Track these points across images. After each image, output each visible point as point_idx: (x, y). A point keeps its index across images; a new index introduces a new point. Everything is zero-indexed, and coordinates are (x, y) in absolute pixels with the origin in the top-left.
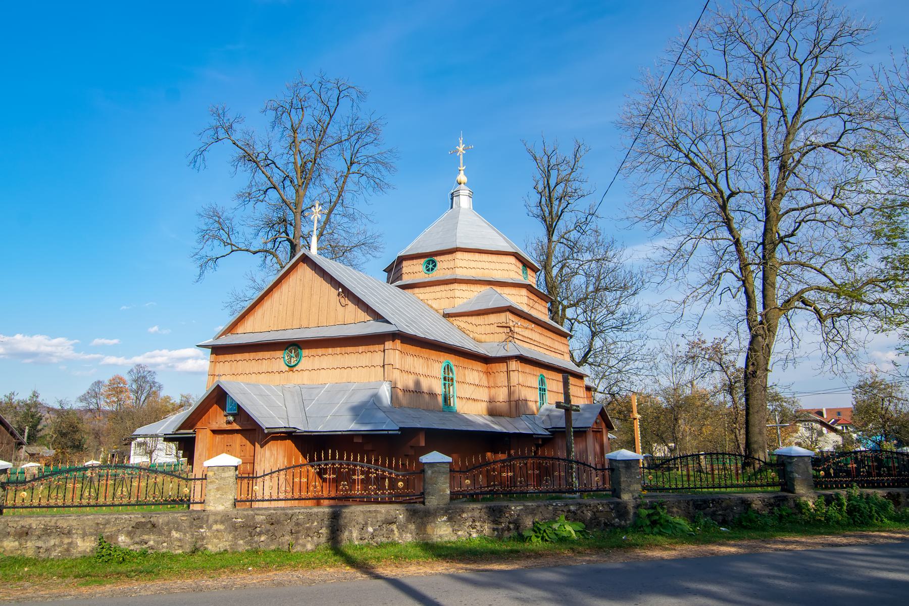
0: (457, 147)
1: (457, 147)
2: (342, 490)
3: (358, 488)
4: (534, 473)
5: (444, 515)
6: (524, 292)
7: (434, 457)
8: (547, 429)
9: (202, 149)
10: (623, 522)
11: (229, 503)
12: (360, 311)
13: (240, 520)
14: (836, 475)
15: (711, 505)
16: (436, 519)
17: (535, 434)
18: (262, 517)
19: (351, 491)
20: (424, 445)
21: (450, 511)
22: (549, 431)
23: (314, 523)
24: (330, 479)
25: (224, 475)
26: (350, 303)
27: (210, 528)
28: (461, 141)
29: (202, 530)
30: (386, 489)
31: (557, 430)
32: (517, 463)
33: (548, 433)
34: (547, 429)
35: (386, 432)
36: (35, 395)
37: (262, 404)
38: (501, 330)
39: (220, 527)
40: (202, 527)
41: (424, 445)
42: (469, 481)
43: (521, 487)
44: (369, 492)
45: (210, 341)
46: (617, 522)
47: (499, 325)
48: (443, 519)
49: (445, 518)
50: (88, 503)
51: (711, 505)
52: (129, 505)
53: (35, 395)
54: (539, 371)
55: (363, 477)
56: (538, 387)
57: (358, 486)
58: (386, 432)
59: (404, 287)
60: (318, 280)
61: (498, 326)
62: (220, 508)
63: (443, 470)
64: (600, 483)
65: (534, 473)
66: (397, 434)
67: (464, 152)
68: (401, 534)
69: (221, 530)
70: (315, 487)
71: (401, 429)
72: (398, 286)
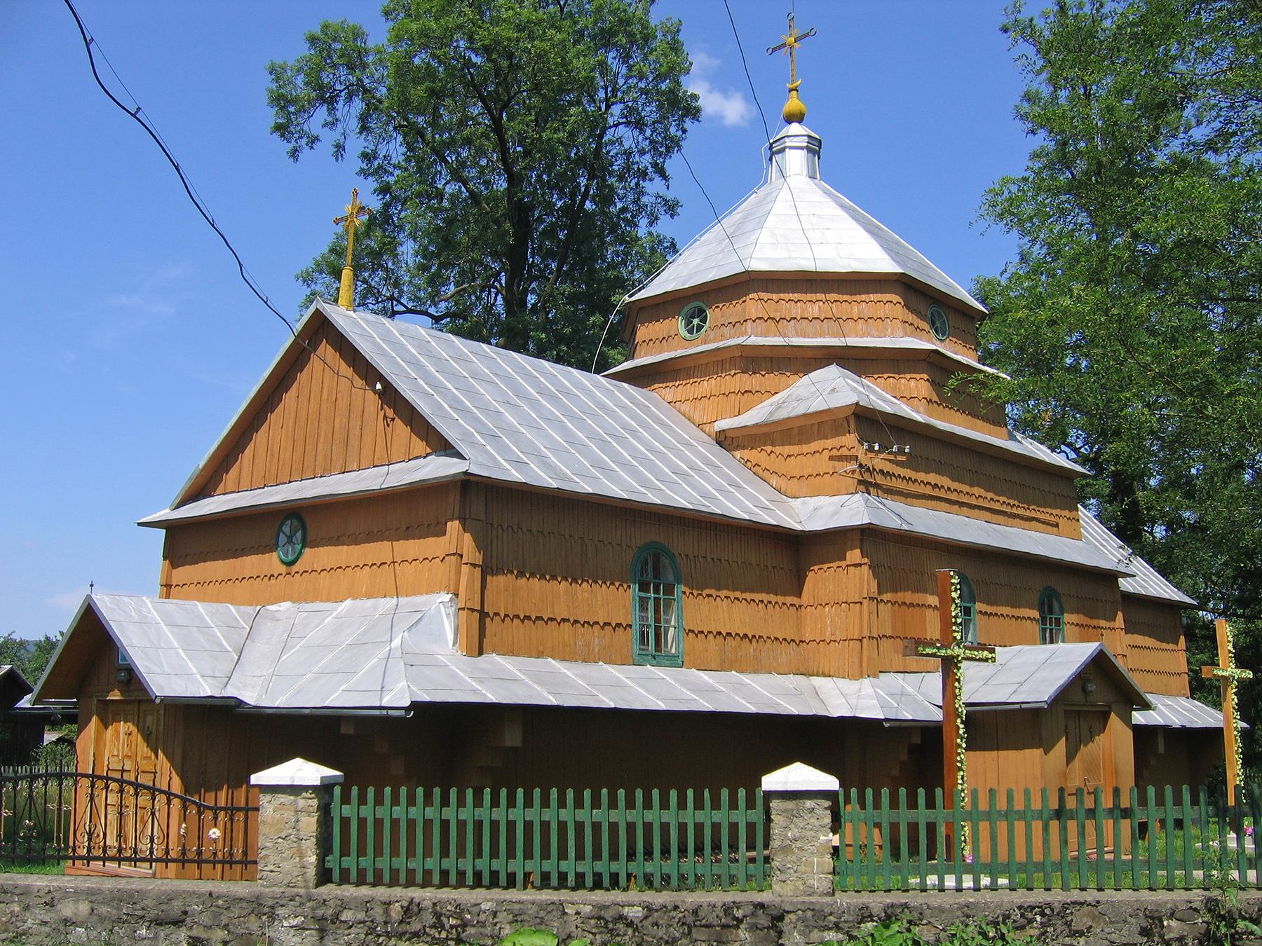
45: (166, 514)
47: (835, 453)
61: (831, 458)
71: (415, 705)
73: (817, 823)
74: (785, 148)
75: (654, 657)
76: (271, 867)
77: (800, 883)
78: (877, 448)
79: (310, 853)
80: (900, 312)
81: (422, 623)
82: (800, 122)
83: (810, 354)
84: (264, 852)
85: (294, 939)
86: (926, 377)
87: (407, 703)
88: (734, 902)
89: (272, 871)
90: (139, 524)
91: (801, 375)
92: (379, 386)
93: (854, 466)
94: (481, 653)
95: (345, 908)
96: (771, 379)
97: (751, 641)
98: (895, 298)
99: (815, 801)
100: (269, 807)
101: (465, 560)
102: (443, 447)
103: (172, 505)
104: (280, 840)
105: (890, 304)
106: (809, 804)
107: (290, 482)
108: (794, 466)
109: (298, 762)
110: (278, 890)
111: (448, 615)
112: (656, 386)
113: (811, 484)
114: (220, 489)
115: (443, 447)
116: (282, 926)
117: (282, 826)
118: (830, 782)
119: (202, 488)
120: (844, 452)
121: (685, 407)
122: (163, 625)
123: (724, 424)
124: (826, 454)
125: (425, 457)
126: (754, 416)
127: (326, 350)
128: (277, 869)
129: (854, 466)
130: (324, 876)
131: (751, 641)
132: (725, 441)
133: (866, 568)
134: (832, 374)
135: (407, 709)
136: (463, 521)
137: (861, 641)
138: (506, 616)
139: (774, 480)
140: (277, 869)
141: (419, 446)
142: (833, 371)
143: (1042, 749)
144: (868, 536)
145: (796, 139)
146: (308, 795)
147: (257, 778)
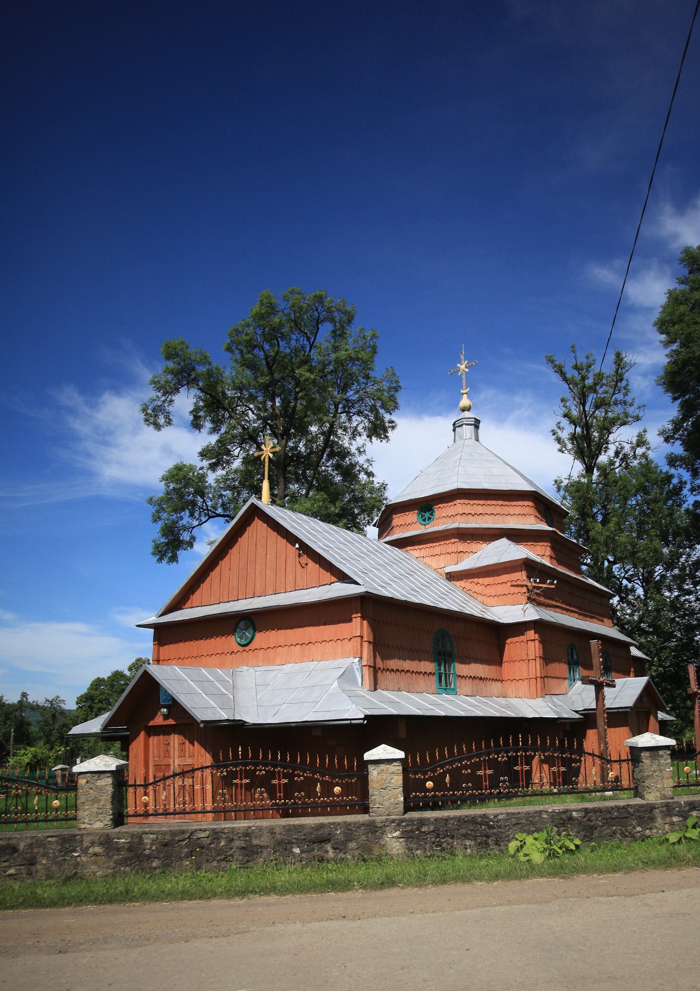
0: (459, 365)
1: (459, 365)
2: (259, 799)
7: (382, 751)
8: (577, 712)
11: (109, 819)
12: (322, 570)
13: (123, 840)
18: (151, 836)
19: (26, 813)
21: (404, 824)
22: (581, 714)
23: (220, 842)
24: (241, 784)
25: (99, 783)
26: (310, 561)
27: (85, 851)
28: (462, 357)
29: (76, 854)
31: (620, 710)
33: (577, 716)
34: (577, 712)
35: (349, 722)
36: (24, 695)
37: (201, 692)
38: (516, 590)
39: (97, 849)
40: (75, 851)
42: (339, 788)
44: (295, 801)
45: (153, 619)
47: (514, 583)
48: (395, 835)
49: (397, 834)
50: (136, 812)
52: (679, 786)
53: (24, 695)
55: (286, 781)
57: (523, 781)
58: (349, 722)
59: (401, 544)
60: (273, 535)
61: (512, 586)
62: (98, 825)
64: (598, 780)
66: (362, 724)
67: (467, 370)
68: (373, 854)
69: (100, 853)
71: (367, 717)
72: (385, 543)
73: (664, 762)
74: (464, 424)
75: (445, 689)
76: (377, 806)
77: (658, 793)
78: (538, 581)
79: (400, 796)
80: (532, 511)
81: (345, 674)
82: (469, 410)
83: (492, 532)
84: (373, 797)
85: (395, 844)
86: (549, 544)
87: (363, 716)
88: (628, 805)
89: (378, 808)
90: (138, 626)
91: (488, 543)
92: (297, 546)
93: (525, 590)
94: (375, 689)
95: (424, 824)
96: (473, 546)
97: (466, 679)
98: (531, 504)
99: (664, 751)
100: (374, 772)
101: (365, 639)
102: (343, 577)
103: (157, 614)
104: (382, 790)
105: (527, 507)
106: (661, 753)
107: (238, 600)
108: (491, 590)
109: (383, 746)
110: (384, 818)
111: (357, 669)
112: (409, 548)
113: (503, 598)
114: (189, 604)
115: (343, 577)
116: (388, 837)
117: (383, 782)
118: (400, 754)
119: (177, 604)
120: (519, 583)
121: (427, 560)
122: (189, 680)
123: (449, 569)
124: (509, 584)
125: (330, 585)
126: (467, 563)
127: (258, 525)
128: (381, 806)
129: (525, 590)
130: (407, 809)
131: (466, 679)
132: (452, 577)
133: (537, 642)
134: (503, 543)
135: (364, 719)
136: (363, 618)
137: (536, 679)
138: (384, 669)
139: (480, 598)
140: (381, 806)
141: (327, 576)
142: (504, 541)
143: (628, 727)
144: (537, 625)
145: (469, 420)
146: (397, 764)
147: (368, 756)
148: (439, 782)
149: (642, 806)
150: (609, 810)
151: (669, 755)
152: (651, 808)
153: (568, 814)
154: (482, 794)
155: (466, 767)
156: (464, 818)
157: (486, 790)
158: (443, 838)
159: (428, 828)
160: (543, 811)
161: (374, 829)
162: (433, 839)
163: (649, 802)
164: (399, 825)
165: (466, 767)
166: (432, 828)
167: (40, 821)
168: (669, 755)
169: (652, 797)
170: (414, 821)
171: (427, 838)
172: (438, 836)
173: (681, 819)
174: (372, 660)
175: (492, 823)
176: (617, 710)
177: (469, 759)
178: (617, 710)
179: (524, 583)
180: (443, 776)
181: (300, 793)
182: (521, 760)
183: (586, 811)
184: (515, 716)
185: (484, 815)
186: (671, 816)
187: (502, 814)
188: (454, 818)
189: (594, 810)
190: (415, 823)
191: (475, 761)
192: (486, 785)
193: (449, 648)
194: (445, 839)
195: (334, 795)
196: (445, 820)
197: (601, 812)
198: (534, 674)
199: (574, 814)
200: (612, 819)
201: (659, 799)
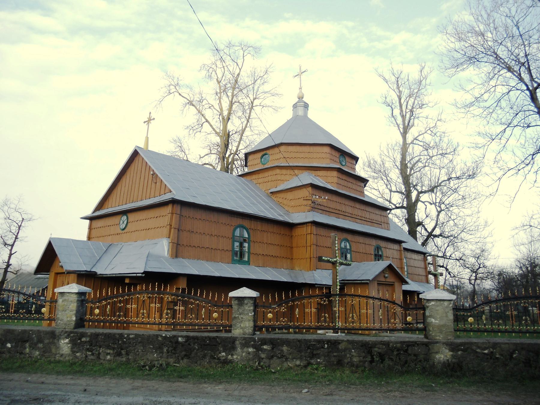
3: (179, 317)
4: (155, 307)
5: (66, 338)
6: (335, 173)
9: (160, 100)
10: (230, 356)
14: (113, 314)
15: (326, 346)
16: (60, 341)
17: (316, 284)
20: (126, 282)
21: (72, 335)
30: (32, 314)
31: (362, 282)
32: (141, 297)
35: (135, 275)
38: (305, 202)
41: (126, 282)
43: (353, 323)
44: (19, 315)
46: (223, 356)
47: (305, 198)
48: (65, 341)
49: (67, 341)
51: (326, 346)
54: (374, 242)
56: (373, 253)
57: (131, 313)
63: (71, 299)
65: (155, 307)
70: (143, 314)
71: (145, 272)
87: (142, 272)
93: (310, 202)
120: (308, 198)
124: (302, 199)
148: (103, 312)
149: (227, 338)
150: (204, 339)
151: (252, 303)
152: (233, 340)
153: (176, 338)
154: (9, 316)
155: (120, 302)
156: (108, 335)
157: (11, 313)
158: (94, 347)
159: (86, 339)
160: (159, 335)
161: (53, 336)
162: (88, 347)
163: (433, 341)
164: (69, 335)
165: (120, 302)
166: (88, 339)
167: (163, 324)
168: (252, 303)
169: (236, 332)
170: (78, 333)
171: (84, 346)
172: (91, 345)
173: (255, 350)
174: (176, 239)
175: (125, 340)
176: (360, 282)
177: (122, 297)
178: (360, 282)
179: (310, 198)
180: (106, 306)
181: (23, 310)
182: (156, 300)
183: (188, 338)
184: (286, 281)
185: (121, 334)
186: (248, 347)
187: (132, 334)
188: (102, 334)
189: (194, 338)
190: (79, 335)
191: (126, 298)
192: (12, 311)
193: (380, 253)
194: (95, 347)
195: (95, 315)
196: (97, 335)
197: (198, 340)
198: (309, 255)
199: (180, 339)
200: (205, 345)
201: (242, 334)
